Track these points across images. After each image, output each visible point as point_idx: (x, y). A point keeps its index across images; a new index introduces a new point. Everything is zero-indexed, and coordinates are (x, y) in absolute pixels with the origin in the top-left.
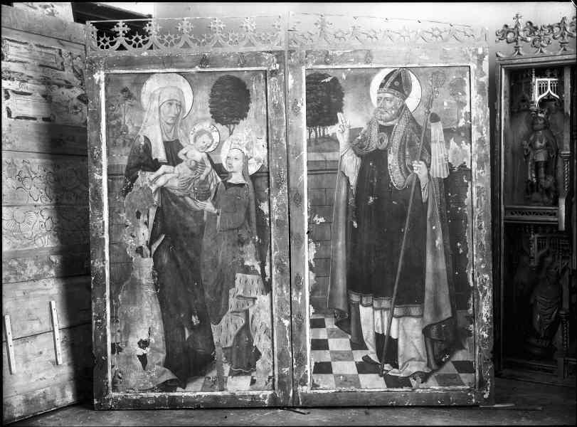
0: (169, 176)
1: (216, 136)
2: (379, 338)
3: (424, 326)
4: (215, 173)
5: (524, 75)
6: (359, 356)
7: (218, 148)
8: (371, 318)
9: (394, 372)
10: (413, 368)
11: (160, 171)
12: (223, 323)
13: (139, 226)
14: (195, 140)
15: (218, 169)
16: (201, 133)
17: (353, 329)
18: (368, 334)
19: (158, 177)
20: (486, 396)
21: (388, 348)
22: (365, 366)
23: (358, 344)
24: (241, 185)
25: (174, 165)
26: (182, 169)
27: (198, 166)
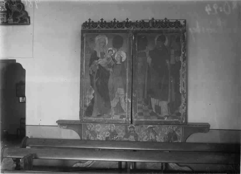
0: (100, 62)
1: (114, 51)
2: (156, 106)
3: (168, 103)
4: (113, 61)
5: (215, 7)
6: (150, 111)
7: (114, 55)
8: (154, 101)
9: (160, 116)
10: (165, 114)
11: (99, 60)
12: (113, 101)
13: (91, 95)
14: (108, 52)
15: (114, 60)
16: (110, 50)
17: (149, 104)
18: (153, 106)
19: (98, 61)
20: (184, 122)
21: (158, 109)
22: (152, 114)
23: (151, 108)
24: (120, 65)
25: (103, 59)
26: (105, 60)
27: (108, 59)
